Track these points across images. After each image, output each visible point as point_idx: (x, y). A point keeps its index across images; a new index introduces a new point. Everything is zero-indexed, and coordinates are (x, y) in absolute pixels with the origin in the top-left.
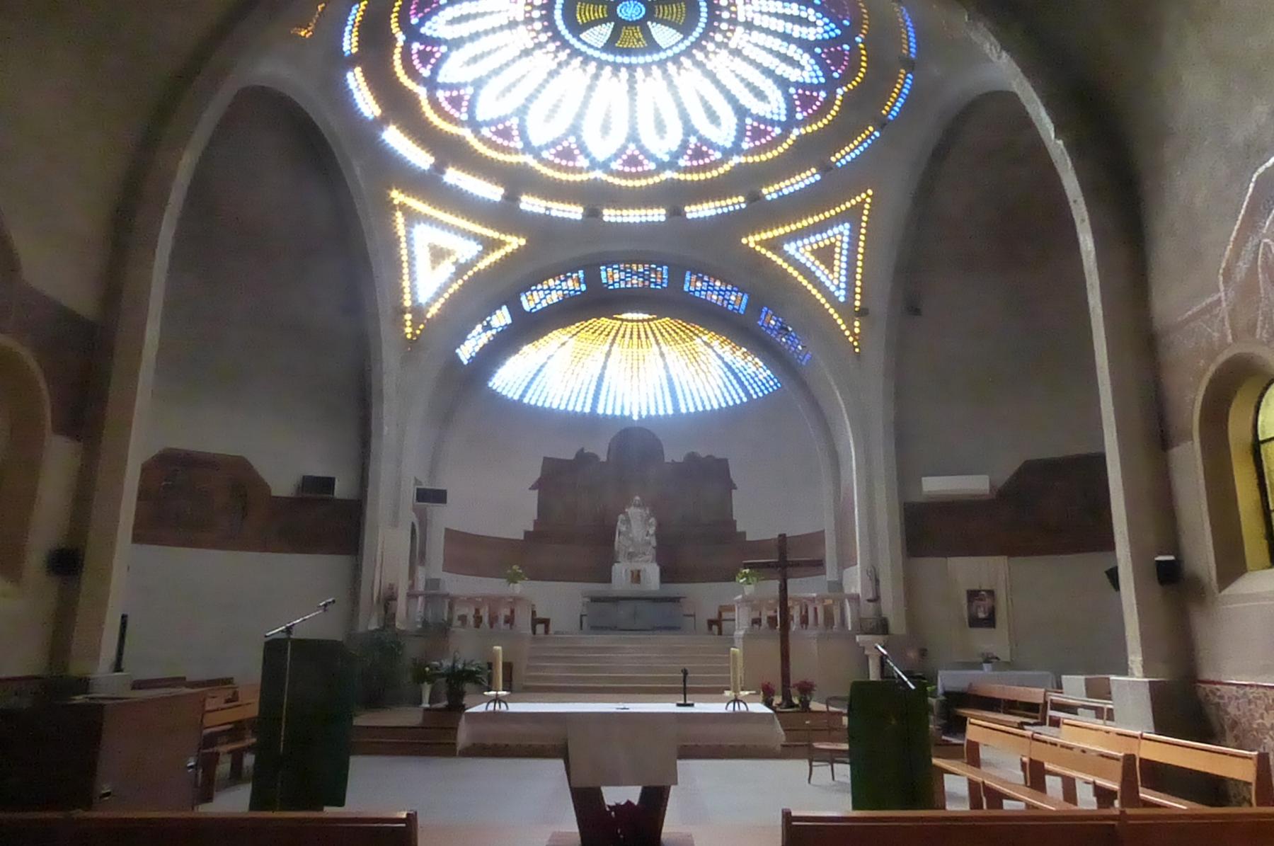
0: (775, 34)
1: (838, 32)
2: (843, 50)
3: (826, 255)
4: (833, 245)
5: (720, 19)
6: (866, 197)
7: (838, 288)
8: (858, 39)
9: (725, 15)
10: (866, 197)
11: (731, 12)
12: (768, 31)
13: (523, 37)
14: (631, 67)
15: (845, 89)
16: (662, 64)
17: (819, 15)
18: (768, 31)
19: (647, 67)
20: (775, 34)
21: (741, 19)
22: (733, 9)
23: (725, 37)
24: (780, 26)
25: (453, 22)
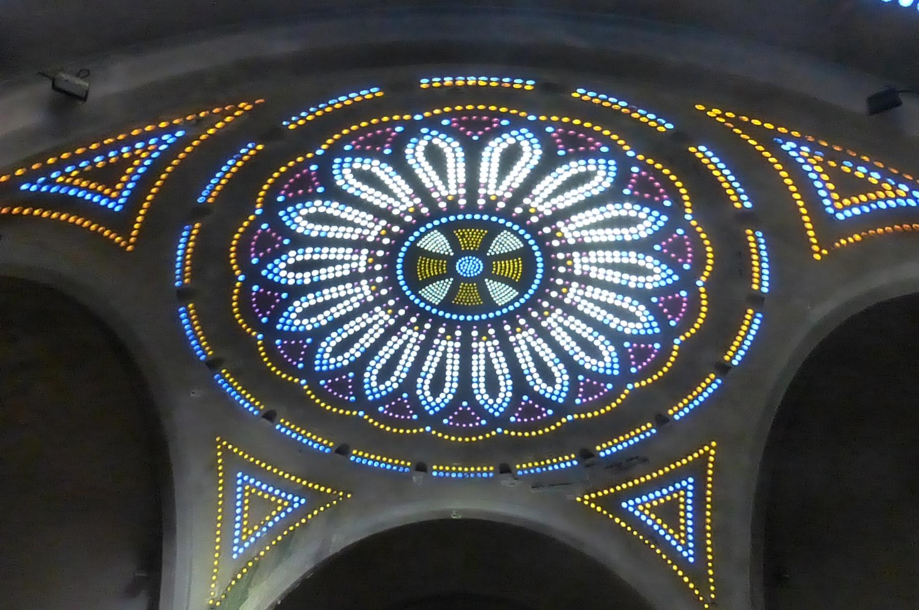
0: (329, 283)
1: (676, 278)
2: (681, 297)
3: (669, 512)
4: (676, 502)
5: (557, 275)
6: (710, 450)
7: (686, 548)
8: (699, 283)
9: (562, 269)
10: (710, 450)
11: (567, 267)
12: (336, 282)
13: (579, 264)
14: (467, 327)
15: (682, 338)
16: (436, 214)
17: (657, 262)
18: (336, 282)
19: (482, 327)
20: (329, 283)
21: (577, 272)
22: (569, 263)
23: (560, 293)
24: (328, 294)
25: (645, 272)
